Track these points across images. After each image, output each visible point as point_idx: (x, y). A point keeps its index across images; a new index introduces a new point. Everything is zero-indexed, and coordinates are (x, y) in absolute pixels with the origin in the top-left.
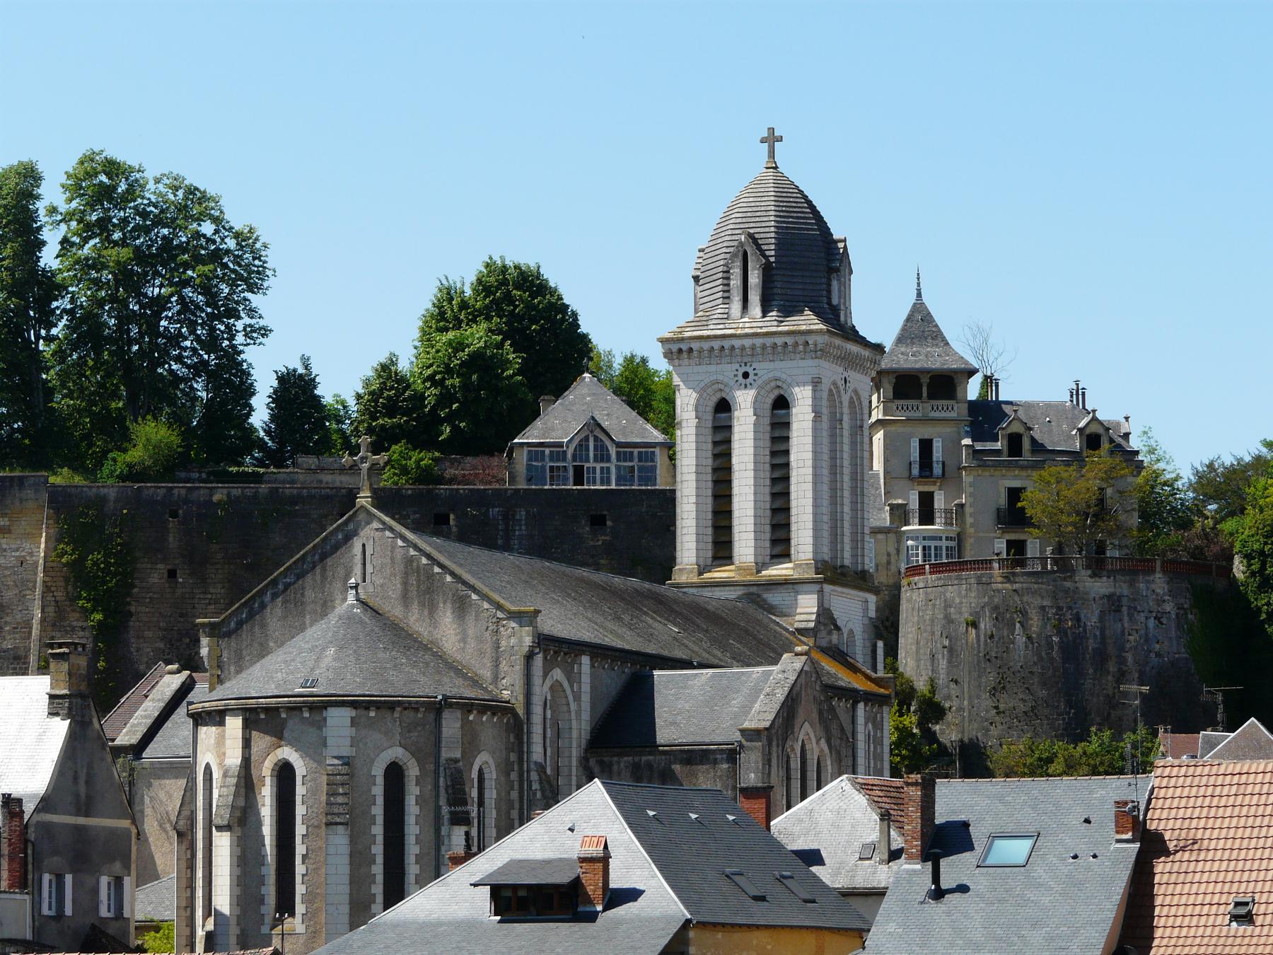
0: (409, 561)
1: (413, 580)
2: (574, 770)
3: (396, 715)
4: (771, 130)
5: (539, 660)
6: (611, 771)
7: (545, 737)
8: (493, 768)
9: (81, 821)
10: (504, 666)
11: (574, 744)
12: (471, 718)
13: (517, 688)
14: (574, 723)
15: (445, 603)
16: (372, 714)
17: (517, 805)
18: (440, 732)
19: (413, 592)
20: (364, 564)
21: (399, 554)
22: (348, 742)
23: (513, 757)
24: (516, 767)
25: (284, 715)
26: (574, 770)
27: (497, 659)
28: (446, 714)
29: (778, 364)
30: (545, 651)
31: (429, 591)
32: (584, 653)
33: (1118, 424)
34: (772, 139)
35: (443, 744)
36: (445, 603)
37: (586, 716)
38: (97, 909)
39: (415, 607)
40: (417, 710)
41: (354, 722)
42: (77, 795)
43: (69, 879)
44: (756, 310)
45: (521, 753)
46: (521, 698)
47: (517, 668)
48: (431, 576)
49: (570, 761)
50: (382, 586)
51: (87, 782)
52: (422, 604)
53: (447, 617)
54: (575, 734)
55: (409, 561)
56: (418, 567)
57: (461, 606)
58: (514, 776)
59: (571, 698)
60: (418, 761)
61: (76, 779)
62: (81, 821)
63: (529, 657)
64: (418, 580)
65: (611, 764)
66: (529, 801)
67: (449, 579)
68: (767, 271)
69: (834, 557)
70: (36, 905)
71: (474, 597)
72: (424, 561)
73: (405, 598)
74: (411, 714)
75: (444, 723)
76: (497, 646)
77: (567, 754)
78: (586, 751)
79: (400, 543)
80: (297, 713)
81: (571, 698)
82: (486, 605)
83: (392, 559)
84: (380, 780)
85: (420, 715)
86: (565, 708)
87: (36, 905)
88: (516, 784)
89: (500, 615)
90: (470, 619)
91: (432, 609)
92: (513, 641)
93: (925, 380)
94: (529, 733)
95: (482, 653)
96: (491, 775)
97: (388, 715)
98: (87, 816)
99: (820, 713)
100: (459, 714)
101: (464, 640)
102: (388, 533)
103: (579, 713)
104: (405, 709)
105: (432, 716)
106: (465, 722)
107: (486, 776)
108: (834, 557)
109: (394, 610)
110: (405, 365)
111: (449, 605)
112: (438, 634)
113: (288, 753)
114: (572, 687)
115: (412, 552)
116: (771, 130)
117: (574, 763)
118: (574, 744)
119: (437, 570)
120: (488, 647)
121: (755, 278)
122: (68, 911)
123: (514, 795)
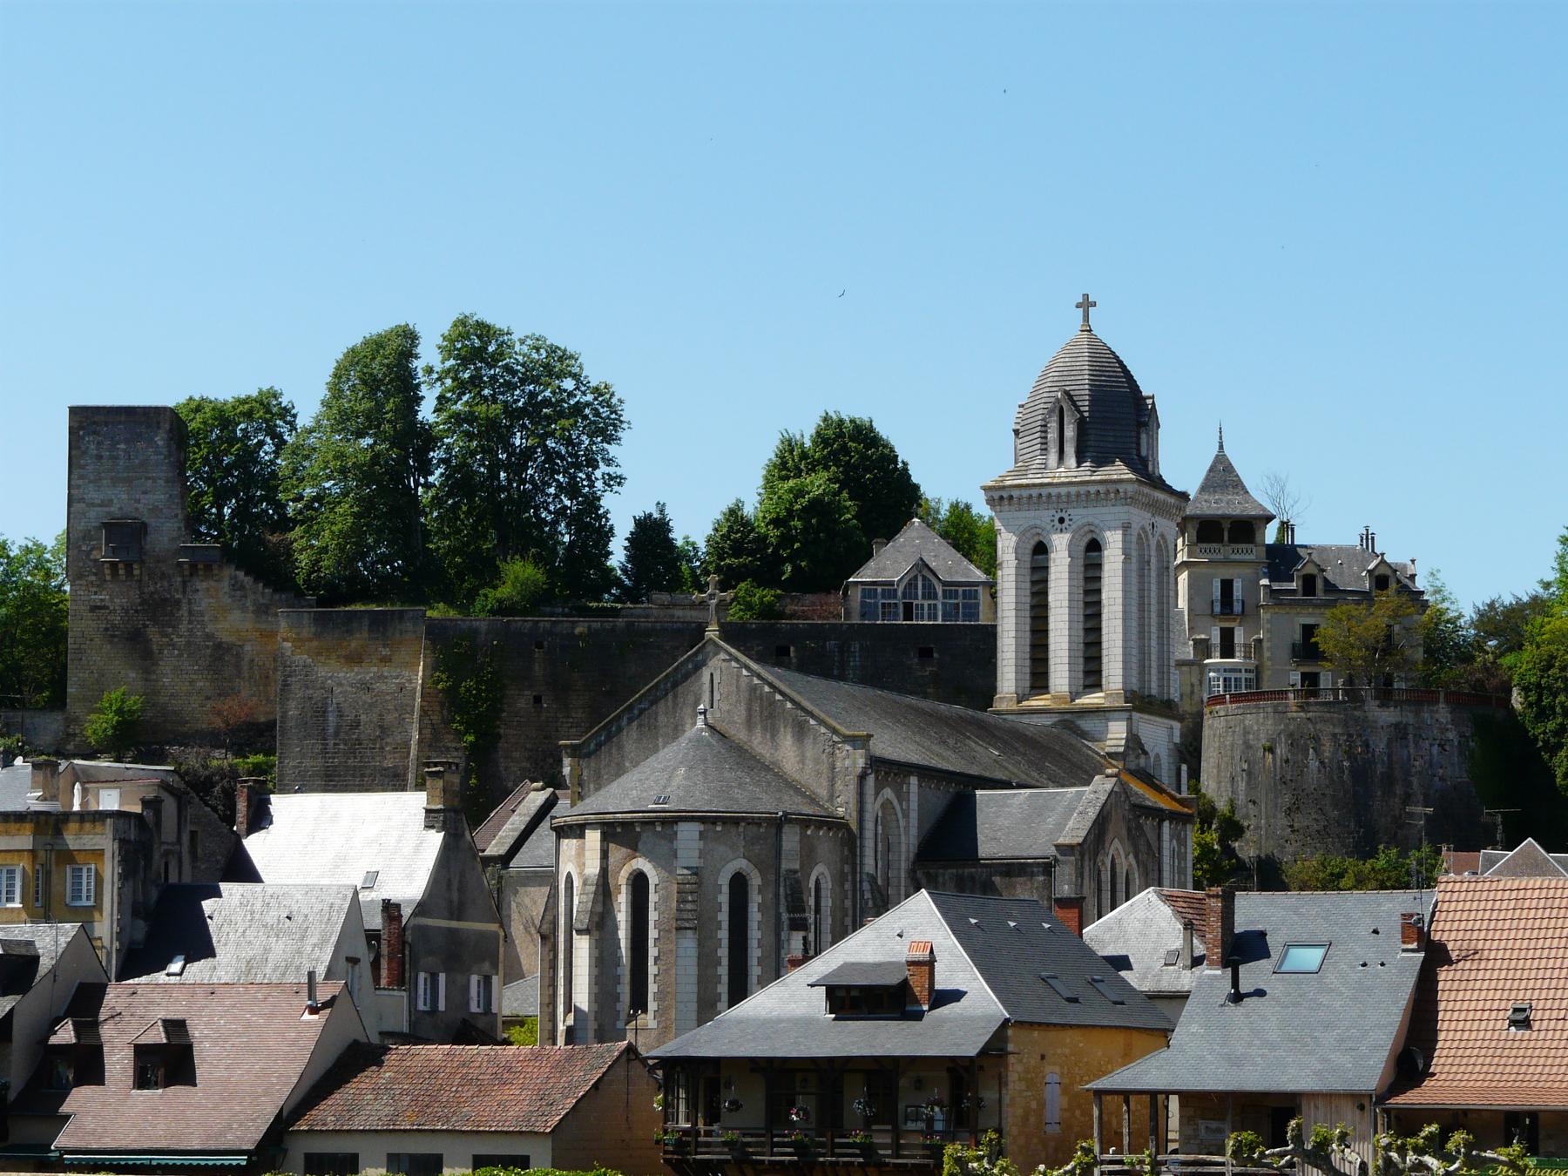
0: (753, 689)
4: (1086, 296)
5: (871, 780)
9: (454, 924)
10: (839, 786)
21: (744, 683)
22: (696, 854)
23: (847, 868)
28: (786, 829)
29: (1091, 511)
30: (877, 772)
31: (771, 716)
32: (911, 773)
33: (1405, 566)
34: (1086, 304)
37: (914, 831)
40: (759, 825)
42: (451, 902)
43: (442, 977)
44: (1071, 461)
46: (854, 814)
48: (773, 703)
52: (765, 729)
53: (787, 741)
54: (904, 848)
57: (801, 731)
58: (848, 886)
62: (454, 924)
63: (862, 778)
67: (789, 705)
68: (1081, 425)
70: (413, 1001)
71: (812, 722)
72: (767, 689)
73: (749, 724)
79: (745, 672)
82: (823, 730)
84: (726, 889)
87: (413, 1001)
88: (850, 894)
89: (835, 738)
90: (809, 741)
92: (847, 762)
93: (1226, 525)
95: (819, 773)
96: (827, 885)
97: (733, 830)
98: (459, 919)
99: (1129, 830)
100: (797, 829)
101: (802, 761)
102: (734, 664)
103: (907, 828)
105: (773, 831)
106: (803, 835)
109: (739, 734)
110: (750, 510)
112: (779, 755)
115: (756, 681)
116: (1086, 296)
119: (778, 697)
120: (824, 768)
121: (1070, 432)
122: (442, 1006)
123: (848, 903)
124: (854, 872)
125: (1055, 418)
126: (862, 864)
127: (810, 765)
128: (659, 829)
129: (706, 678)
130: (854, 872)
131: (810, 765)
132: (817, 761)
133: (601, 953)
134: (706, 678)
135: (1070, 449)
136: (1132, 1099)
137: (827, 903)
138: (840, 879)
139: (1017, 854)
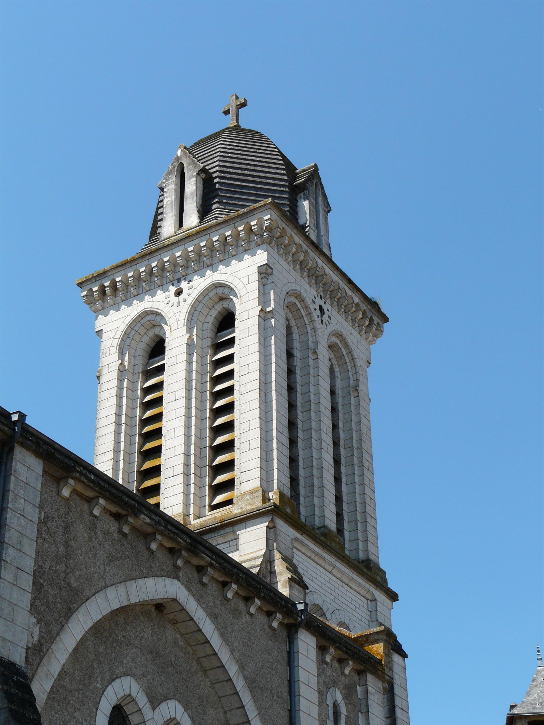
121: (192, 186)
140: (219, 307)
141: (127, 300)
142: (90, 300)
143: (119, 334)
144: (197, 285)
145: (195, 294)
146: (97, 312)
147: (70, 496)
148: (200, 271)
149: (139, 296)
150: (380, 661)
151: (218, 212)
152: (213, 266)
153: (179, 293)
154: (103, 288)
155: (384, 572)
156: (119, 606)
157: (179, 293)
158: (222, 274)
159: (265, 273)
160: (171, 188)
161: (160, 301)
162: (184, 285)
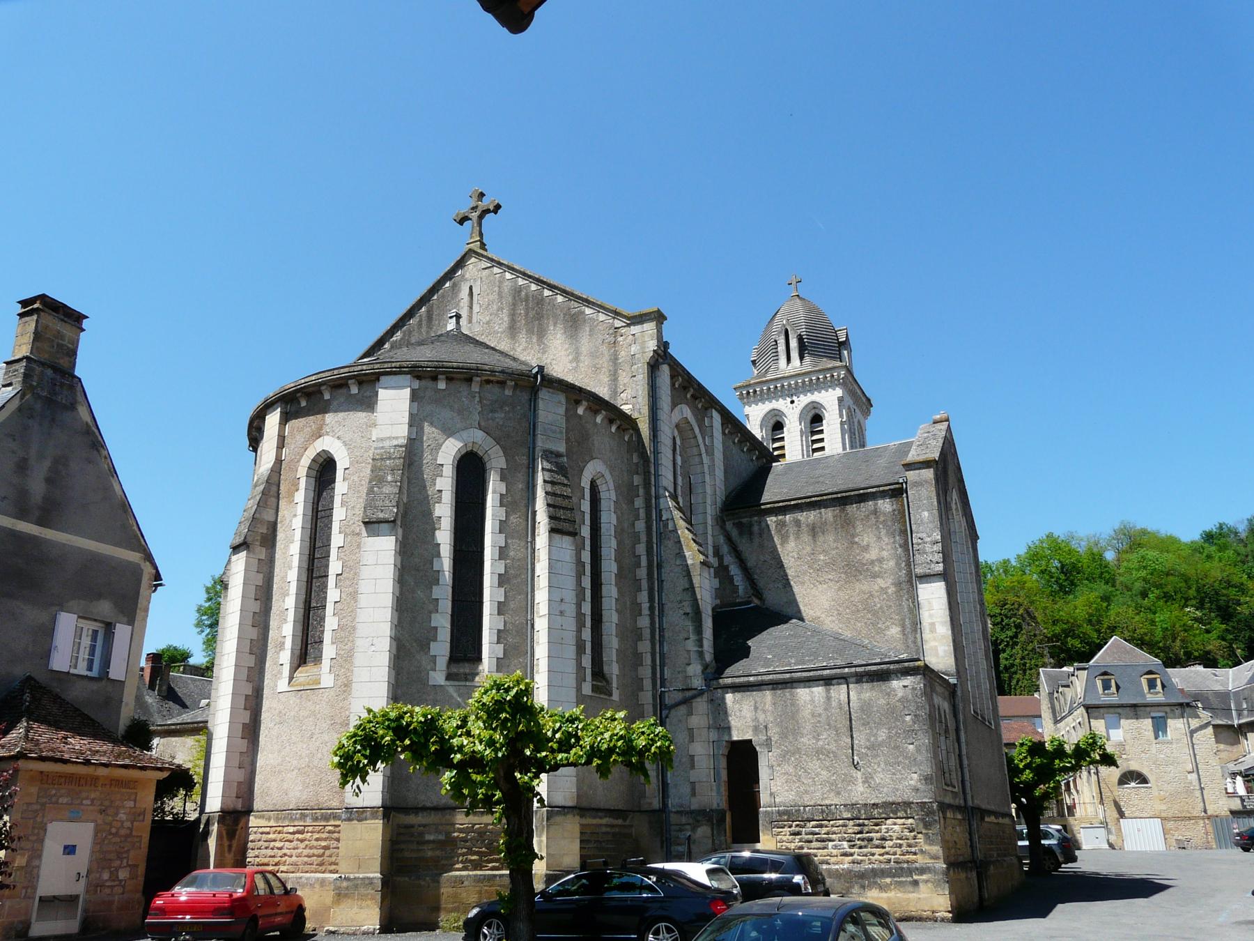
0: (517, 291)
1: (521, 310)
2: (709, 528)
3: (475, 387)
6: (751, 533)
7: (674, 450)
8: (612, 486)
10: (624, 378)
11: (709, 501)
12: (580, 411)
13: (640, 400)
14: (707, 478)
15: (555, 324)
16: (442, 385)
17: (643, 538)
18: (535, 416)
19: (521, 322)
20: (471, 308)
21: (507, 287)
23: (637, 480)
24: (641, 491)
25: (327, 396)
26: (709, 528)
27: (616, 371)
28: (544, 394)
31: (539, 317)
35: (539, 432)
36: (555, 324)
37: (720, 473)
38: (47, 655)
39: (522, 337)
40: (502, 383)
41: (414, 397)
45: (647, 474)
46: (645, 410)
47: (640, 377)
48: (540, 301)
49: (705, 519)
50: (488, 323)
51: (49, 481)
52: (530, 332)
54: (709, 490)
55: (517, 291)
56: (527, 295)
57: (574, 323)
58: (639, 502)
59: (703, 450)
60: (504, 449)
61: (22, 467)
64: (527, 309)
65: (751, 525)
66: (660, 535)
67: (560, 299)
69: (828, 691)
71: (588, 311)
72: (534, 287)
73: (513, 330)
74: (496, 389)
75: (541, 404)
76: (615, 359)
77: (701, 510)
78: (722, 510)
79: (508, 276)
80: (344, 391)
81: (703, 450)
82: (602, 317)
83: (500, 294)
84: (449, 472)
85: (508, 392)
86: (697, 459)
88: (642, 513)
89: (618, 323)
91: (542, 334)
92: (634, 349)
94: (657, 465)
95: (596, 369)
96: (608, 496)
97: (463, 388)
98: (40, 523)
101: (576, 359)
102: (496, 270)
103: (712, 467)
104: (488, 382)
105: (525, 397)
106: (570, 415)
107: (603, 495)
108: (828, 691)
111: (560, 326)
113: (328, 444)
114: (704, 439)
115: (521, 282)
117: (709, 522)
118: (709, 501)
119: (547, 293)
120: (604, 362)
121: (794, 343)
123: (640, 526)
124: (647, 485)
125: (783, 337)
126: (657, 476)
127: (586, 361)
128: (442, 385)
129: (464, 293)
130: (647, 485)
131: (586, 361)
132: (594, 355)
133: (397, 679)
134: (464, 293)
135: (795, 354)
136: (1194, 776)
137: (609, 519)
138: (626, 493)
139: (851, 486)
140: (813, 412)
141: (762, 400)
142: (741, 397)
143: (760, 419)
144: (803, 400)
145: (803, 405)
146: (744, 404)
147: (54, 620)
148: (805, 392)
149: (769, 399)
150: (150, 749)
151: (807, 359)
152: (819, 389)
153: (792, 402)
154: (797, 383)
155: (1171, 537)
156: (66, 670)
157: (792, 402)
158: (817, 397)
159: (840, 400)
160: (782, 341)
161: (781, 404)
162: (795, 398)
